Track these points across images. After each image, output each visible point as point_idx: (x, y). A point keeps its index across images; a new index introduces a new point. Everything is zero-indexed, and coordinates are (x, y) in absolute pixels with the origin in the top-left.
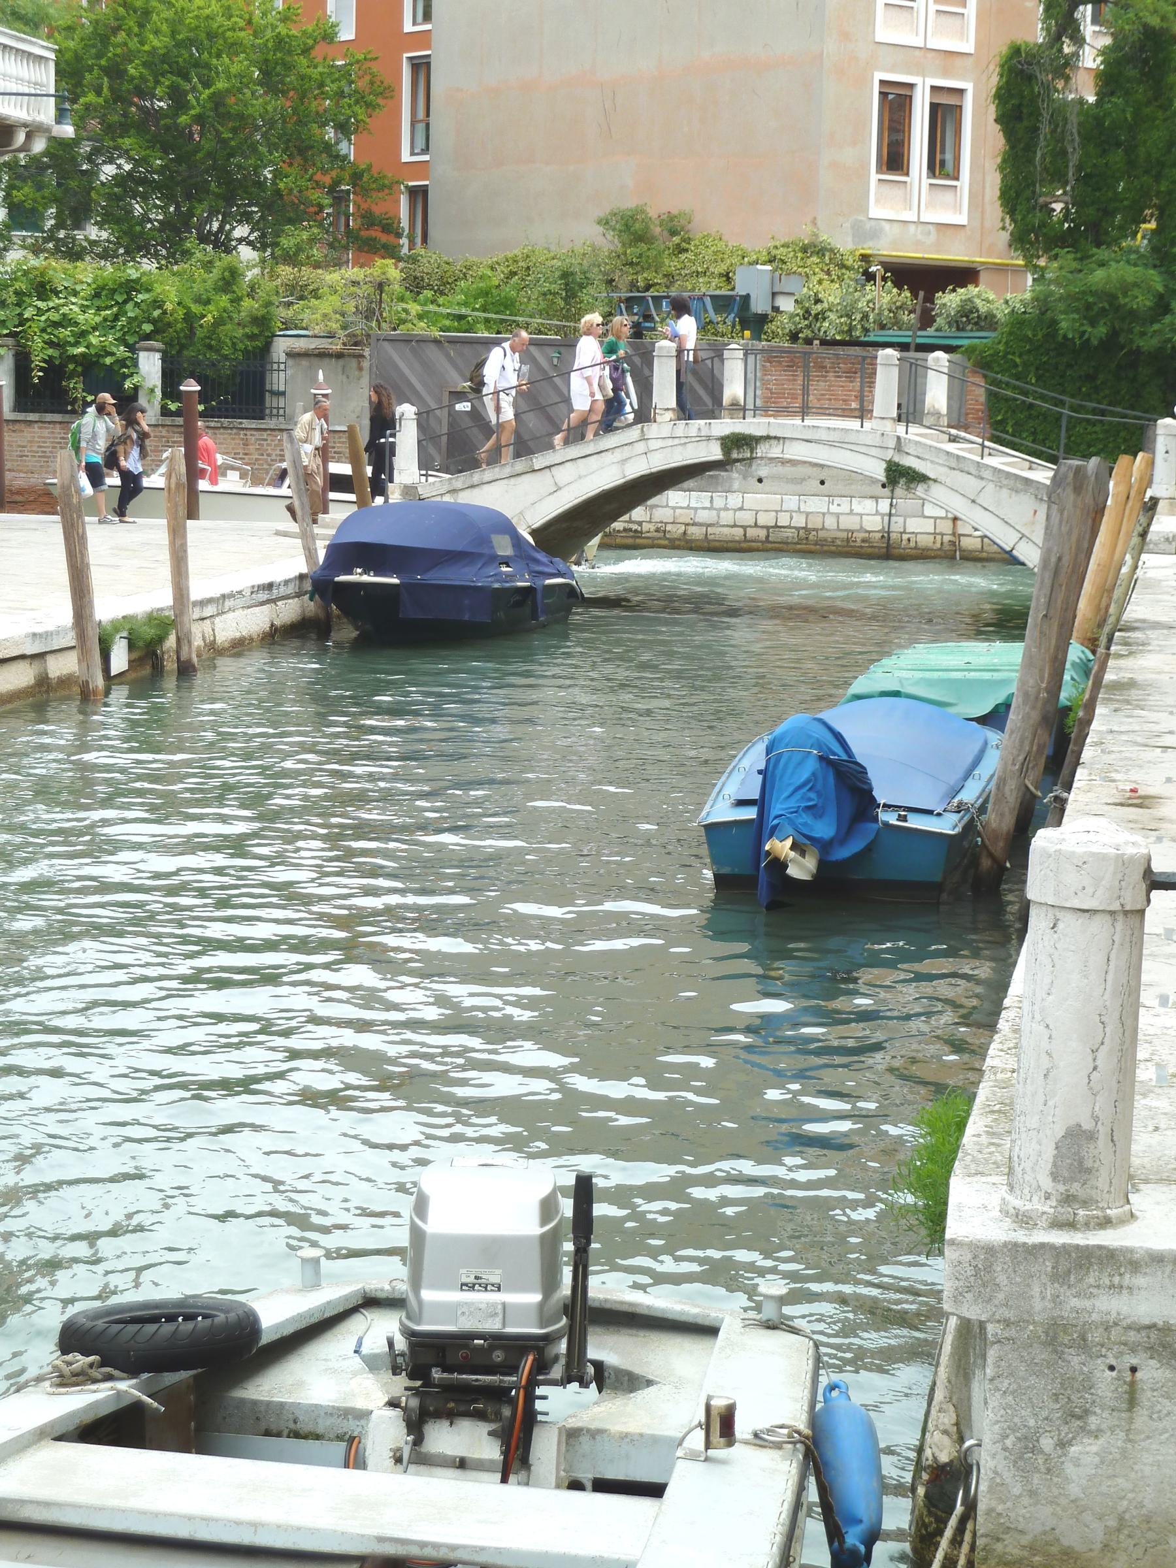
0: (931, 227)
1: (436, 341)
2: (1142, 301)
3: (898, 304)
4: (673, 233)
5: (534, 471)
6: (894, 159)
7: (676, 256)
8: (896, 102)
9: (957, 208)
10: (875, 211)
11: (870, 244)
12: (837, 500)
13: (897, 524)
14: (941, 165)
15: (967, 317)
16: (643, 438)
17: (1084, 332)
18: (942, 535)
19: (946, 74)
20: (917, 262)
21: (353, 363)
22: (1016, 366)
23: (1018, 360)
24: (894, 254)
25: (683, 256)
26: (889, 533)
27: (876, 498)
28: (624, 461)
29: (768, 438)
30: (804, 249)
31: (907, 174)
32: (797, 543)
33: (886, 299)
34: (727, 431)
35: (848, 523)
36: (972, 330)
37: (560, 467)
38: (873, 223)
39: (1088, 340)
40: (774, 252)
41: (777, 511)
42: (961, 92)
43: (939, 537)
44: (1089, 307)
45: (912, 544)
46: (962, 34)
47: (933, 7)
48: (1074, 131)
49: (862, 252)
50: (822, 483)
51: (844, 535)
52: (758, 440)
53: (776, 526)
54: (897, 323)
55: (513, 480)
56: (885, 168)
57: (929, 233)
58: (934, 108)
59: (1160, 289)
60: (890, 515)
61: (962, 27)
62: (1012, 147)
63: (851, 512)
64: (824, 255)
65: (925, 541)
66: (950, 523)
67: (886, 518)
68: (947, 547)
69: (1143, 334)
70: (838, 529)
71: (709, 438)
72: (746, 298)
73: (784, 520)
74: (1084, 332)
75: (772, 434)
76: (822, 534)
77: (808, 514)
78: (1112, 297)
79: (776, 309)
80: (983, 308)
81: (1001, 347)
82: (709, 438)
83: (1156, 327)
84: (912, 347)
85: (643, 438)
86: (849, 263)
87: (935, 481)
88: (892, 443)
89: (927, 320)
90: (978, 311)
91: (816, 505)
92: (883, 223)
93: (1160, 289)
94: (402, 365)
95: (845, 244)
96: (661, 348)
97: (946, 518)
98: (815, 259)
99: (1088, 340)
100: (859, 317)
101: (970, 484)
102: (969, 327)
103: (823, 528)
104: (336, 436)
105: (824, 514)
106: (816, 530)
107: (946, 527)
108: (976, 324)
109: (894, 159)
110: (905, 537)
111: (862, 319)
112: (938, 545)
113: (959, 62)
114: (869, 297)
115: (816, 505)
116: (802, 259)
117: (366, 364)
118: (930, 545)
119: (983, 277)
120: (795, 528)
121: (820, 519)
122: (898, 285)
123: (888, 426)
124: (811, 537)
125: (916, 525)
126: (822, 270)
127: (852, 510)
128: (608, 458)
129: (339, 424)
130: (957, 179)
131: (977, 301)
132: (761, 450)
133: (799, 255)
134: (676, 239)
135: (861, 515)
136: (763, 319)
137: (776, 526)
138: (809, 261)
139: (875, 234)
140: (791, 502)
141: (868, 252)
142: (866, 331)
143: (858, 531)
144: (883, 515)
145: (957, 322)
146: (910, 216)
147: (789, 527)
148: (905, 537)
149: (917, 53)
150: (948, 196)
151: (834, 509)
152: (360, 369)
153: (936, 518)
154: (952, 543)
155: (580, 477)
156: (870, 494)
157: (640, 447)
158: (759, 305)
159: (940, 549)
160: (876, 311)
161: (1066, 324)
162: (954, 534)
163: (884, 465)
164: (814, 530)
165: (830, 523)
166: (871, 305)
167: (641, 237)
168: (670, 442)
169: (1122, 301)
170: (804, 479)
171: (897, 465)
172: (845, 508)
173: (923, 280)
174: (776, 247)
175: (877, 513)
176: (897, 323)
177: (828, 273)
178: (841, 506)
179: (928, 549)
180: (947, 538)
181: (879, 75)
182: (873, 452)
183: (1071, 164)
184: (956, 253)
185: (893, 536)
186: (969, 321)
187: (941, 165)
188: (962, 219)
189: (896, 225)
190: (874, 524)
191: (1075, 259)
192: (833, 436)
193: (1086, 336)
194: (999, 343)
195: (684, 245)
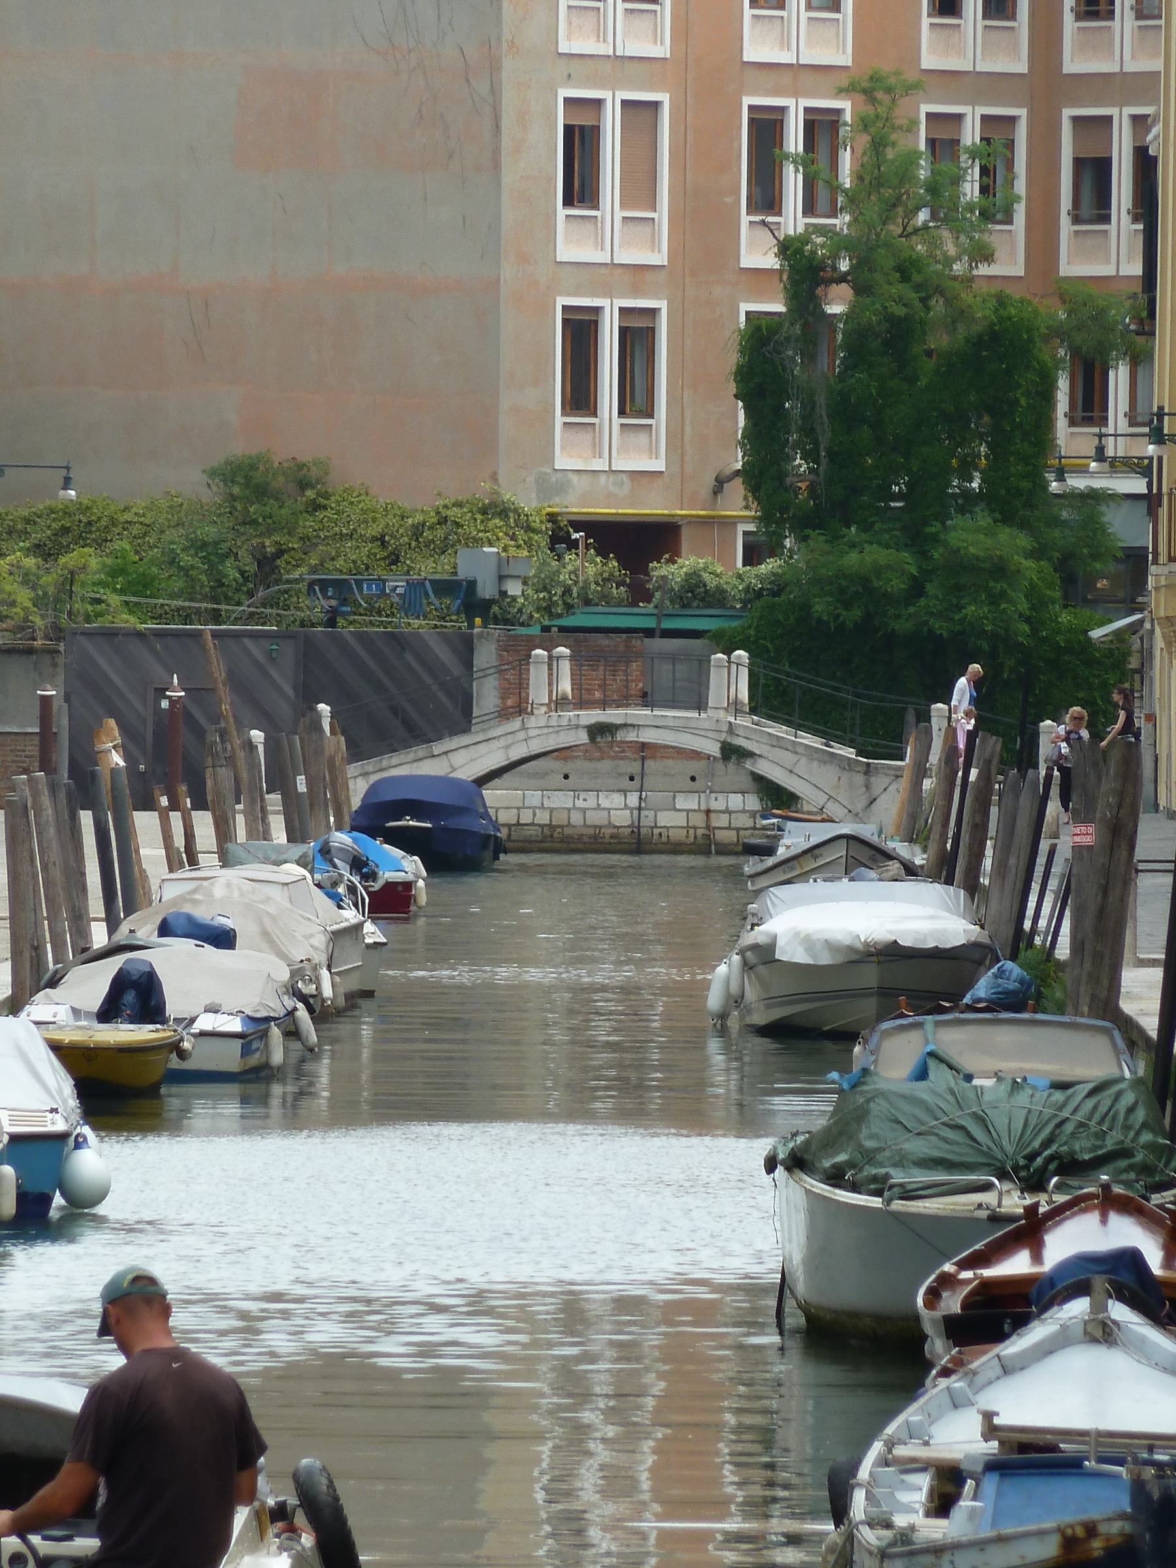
0: (623, 476)
1: (140, 635)
2: (897, 584)
3: (606, 575)
4: (303, 485)
5: (434, 756)
6: (580, 397)
7: (311, 513)
8: (581, 331)
9: (653, 452)
10: (562, 462)
11: (557, 500)
12: (583, 795)
13: (648, 818)
14: (636, 401)
15: (692, 591)
16: (524, 728)
17: (838, 615)
18: (695, 828)
19: (636, 292)
20: (610, 519)
21: (47, 659)
22: (768, 651)
23: (770, 645)
24: (585, 510)
25: (320, 514)
26: (639, 827)
27: (625, 792)
28: (507, 747)
29: (625, 725)
30: (484, 511)
31: (595, 415)
32: (541, 842)
33: (591, 570)
34: (593, 721)
35: (594, 818)
36: (698, 607)
37: (455, 753)
38: (559, 475)
39: (844, 622)
40: (444, 513)
41: (518, 808)
42: (653, 312)
43: (691, 831)
44: (842, 590)
45: (664, 839)
46: (653, 242)
47: (619, 214)
48: (824, 414)
49: (549, 510)
50: (566, 777)
51: (591, 831)
52: (617, 727)
53: (518, 824)
54: (606, 598)
55: (415, 764)
56: (568, 408)
57: (622, 483)
58: (623, 331)
59: (913, 570)
60: (640, 809)
61: (653, 234)
62: (755, 425)
63: (599, 807)
64: (507, 516)
65: (677, 835)
66: (703, 816)
67: (636, 813)
68: (700, 841)
69: (898, 617)
70: (585, 825)
71: (577, 727)
72: (472, 584)
73: (526, 817)
74: (838, 615)
75: (629, 722)
76: (567, 831)
77: (552, 810)
78: (865, 581)
79: (504, 594)
80: (711, 582)
81: (752, 632)
82: (577, 727)
83: (911, 610)
84: (658, 632)
85: (524, 728)
86: (537, 525)
87: (760, 756)
88: (725, 728)
89: (639, 593)
90: (705, 586)
91: (561, 800)
92: (570, 475)
93: (913, 570)
94: (101, 661)
95: (528, 502)
96: (536, 655)
97: (699, 810)
98: (497, 521)
99: (844, 622)
100: (559, 591)
101: (787, 757)
102: (695, 604)
103: (569, 825)
104: (28, 738)
105: (569, 810)
106: (562, 827)
107: (698, 820)
108: (702, 600)
109: (580, 397)
110: (656, 831)
111: (564, 594)
112: (692, 840)
113: (649, 276)
114: (570, 567)
115: (561, 800)
116: (482, 521)
117: (61, 660)
118: (684, 839)
119: (686, 535)
120: (539, 825)
121: (565, 815)
122: (602, 552)
123: (722, 714)
124: (556, 835)
125: (666, 819)
126: (506, 534)
127: (599, 805)
128: (494, 744)
129: (32, 726)
130: (651, 416)
131: (705, 575)
132: (620, 736)
133: (479, 517)
134: (310, 494)
135: (609, 810)
136: (489, 603)
137: (518, 824)
138: (490, 524)
139: (561, 488)
140: (534, 798)
141: (555, 510)
142: (569, 607)
143: (606, 827)
144: (632, 809)
145: (681, 598)
146: (600, 465)
147: (532, 824)
148: (656, 831)
149: (604, 270)
150: (642, 438)
151: (580, 803)
152: (55, 665)
153: (688, 811)
154: (707, 837)
155: (472, 760)
156: (616, 788)
157: (522, 735)
158: (486, 590)
159: (694, 844)
160: (581, 584)
161: (820, 607)
162: (708, 827)
163: (719, 745)
164: (559, 826)
165: (576, 818)
166: (573, 577)
167: (261, 492)
168: (546, 730)
169: (876, 584)
170: (546, 774)
171: (730, 744)
172: (591, 802)
173: (635, 543)
174: (446, 507)
175: (626, 807)
176: (606, 598)
177: (513, 538)
178: (587, 801)
179: (680, 844)
180: (700, 832)
181: (562, 301)
182: (710, 734)
183: (822, 447)
184: (653, 506)
185: (644, 831)
186: (695, 597)
187: (636, 401)
188: (659, 465)
189: (584, 476)
190: (622, 818)
191: (826, 542)
192: (678, 723)
193: (841, 619)
194: (750, 627)
195: (322, 501)
